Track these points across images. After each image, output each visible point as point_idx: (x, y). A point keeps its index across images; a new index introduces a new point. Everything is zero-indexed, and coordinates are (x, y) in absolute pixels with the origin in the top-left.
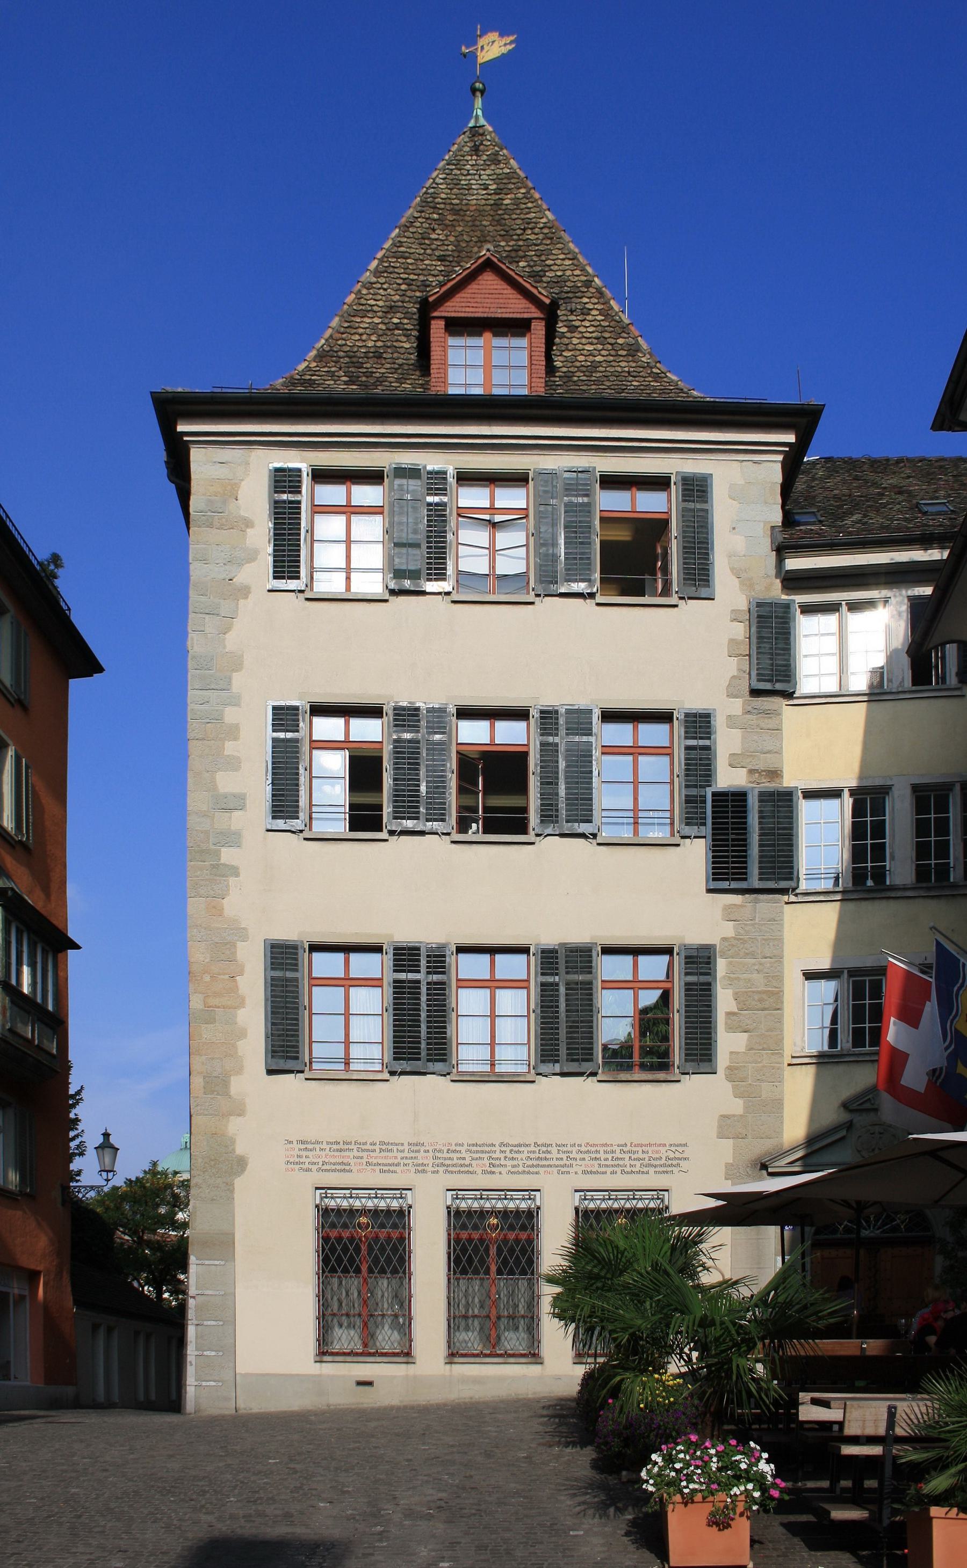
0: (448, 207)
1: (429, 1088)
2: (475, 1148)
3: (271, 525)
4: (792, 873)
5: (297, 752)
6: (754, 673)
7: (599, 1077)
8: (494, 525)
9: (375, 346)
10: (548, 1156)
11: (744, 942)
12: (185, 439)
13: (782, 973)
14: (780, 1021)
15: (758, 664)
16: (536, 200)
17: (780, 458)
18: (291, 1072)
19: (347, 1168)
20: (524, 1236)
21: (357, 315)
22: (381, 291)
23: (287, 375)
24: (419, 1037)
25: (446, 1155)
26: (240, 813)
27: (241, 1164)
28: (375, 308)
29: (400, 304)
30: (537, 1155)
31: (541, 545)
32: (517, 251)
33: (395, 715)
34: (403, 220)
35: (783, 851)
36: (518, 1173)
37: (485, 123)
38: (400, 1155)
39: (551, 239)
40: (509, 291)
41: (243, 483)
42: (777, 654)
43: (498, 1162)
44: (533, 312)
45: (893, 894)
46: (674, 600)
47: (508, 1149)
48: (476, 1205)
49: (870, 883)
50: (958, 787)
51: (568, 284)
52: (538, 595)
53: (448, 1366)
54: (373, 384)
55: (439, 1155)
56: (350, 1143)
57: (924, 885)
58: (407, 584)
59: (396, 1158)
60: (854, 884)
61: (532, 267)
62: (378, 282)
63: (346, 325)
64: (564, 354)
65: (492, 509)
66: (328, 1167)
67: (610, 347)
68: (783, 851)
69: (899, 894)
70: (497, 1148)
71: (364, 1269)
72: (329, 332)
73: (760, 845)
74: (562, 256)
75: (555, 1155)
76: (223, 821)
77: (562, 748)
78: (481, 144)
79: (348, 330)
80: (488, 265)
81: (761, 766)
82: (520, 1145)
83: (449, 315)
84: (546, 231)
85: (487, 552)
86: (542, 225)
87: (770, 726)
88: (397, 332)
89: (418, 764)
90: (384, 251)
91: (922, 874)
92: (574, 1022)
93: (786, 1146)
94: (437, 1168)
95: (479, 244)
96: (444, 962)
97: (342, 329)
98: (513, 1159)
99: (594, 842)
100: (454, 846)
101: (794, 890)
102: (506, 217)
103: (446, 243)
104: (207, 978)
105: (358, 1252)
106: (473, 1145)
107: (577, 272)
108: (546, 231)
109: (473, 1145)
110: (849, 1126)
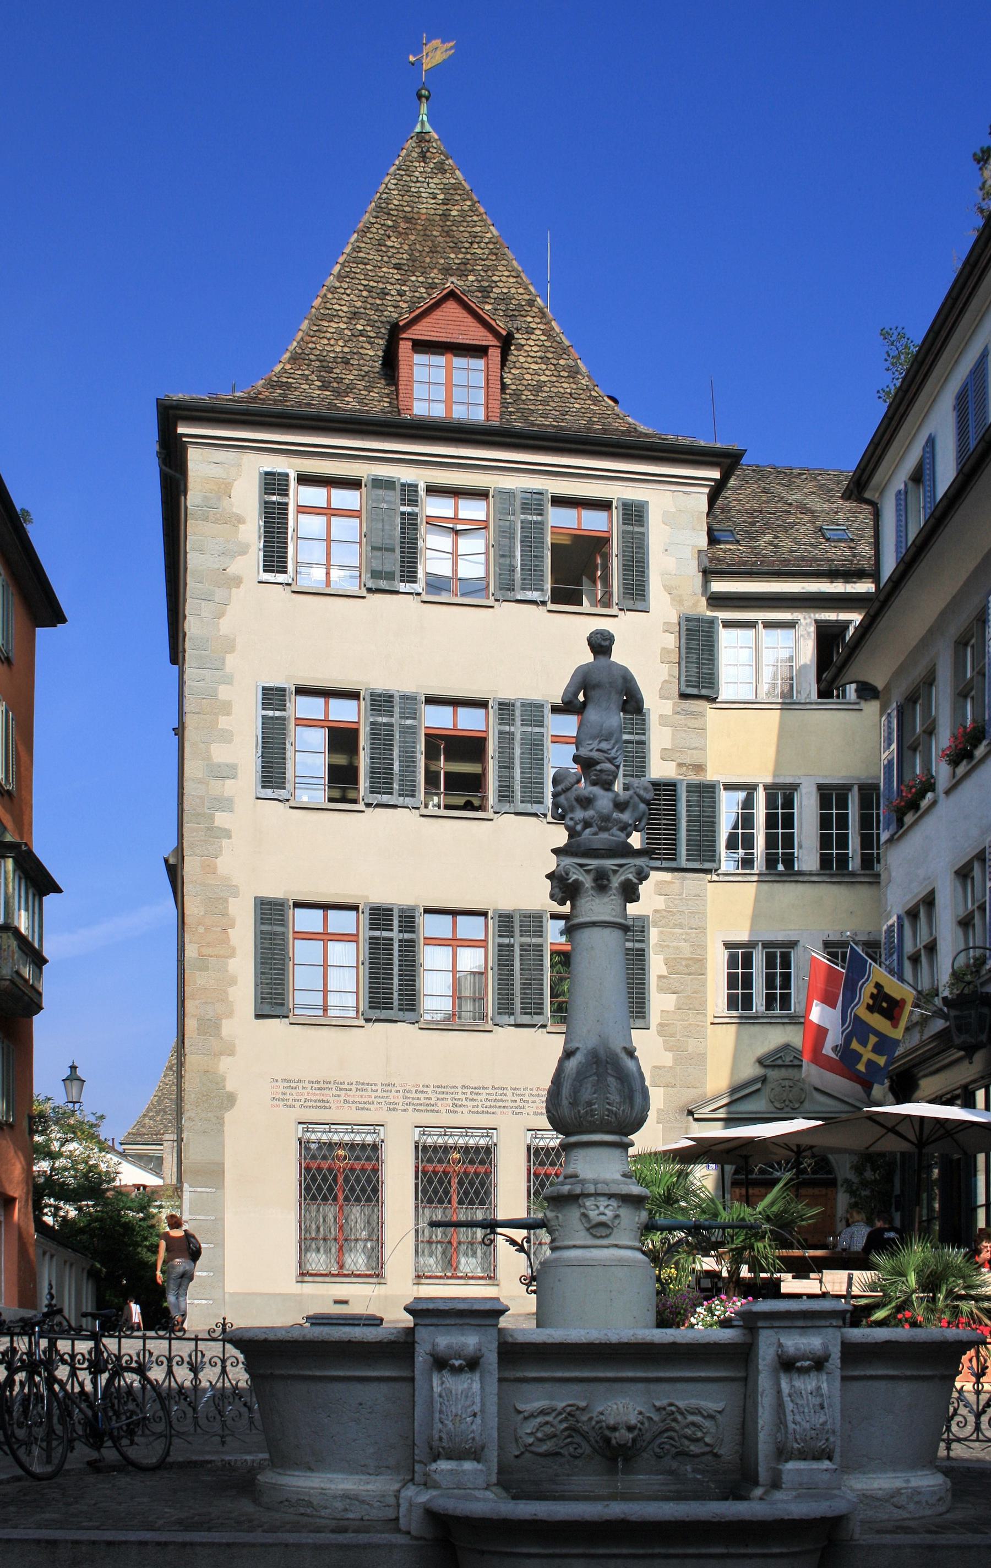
0: (401, 214)
1: (396, 1036)
2: (440, 1090)
3: (262, 523)
4: (714, 856)
5: (284, 729)
6: (683, 678)
7: (549, 1029)
8: (457, 533)
9: (342, 352)
10: (504, 1098)
11: (674, 914)
12: (184, 439)
13: (706, 942)
14: (704, 984)
15: (687, 671)
16: (481, 214)
17: (707, 490)
18: (278, 1017)
19: (327, 1105)
20: (482, 1169)
21: (328, 323)
22: (345, 296)
23: (266, 376)
24: (390, 989)
25: (414, 1095)
26: (233, 781)
27: (231, 1099)
28: (340, 313)
29: (362, 310)
30: (494, 1097)
31: (500, 552)
32: (465, 264)
33: (372, 700)
34: (361, 225)
35: (707, 836)
36: (478, 1112)
37: (431, 130)
38: (374, 1094)
39: (496, 254)
40: (469, 320)
41: (236, 483)
42: (703, 664)
43: (460, 1103)
44: (490, 340)
45: (801, 879)
46: (614, 611)
47: (469, 1091)
48: (440, 1141)
49: (781, 867)
50: (856, 789)
51: (513, 301)
52: (497, 600)
53: (416, 1287)
54: (345, 391)
55: (409, 1095)
56: (330, 1083)
57: (828, 872)
58: (383, 584)
59: (370, 1096)
60: (767, 868)
61: (480, 281)
62: (341, 287)
63: (315, 328)
64: (513, 371)
65: (456, 519)
66: (310, 1104)
67: (553, 368)
68: (707, 836)
69: (806, 879)
70: (459, 1090)
71: (341, 1197)
72: (300, 334)
73: (688, 831)
74: (506, 273)
75: (510, 1097)
76: (216, 787)
77: (518, 737)
78: (428, 151)
79: (317, 334)
80: (452, 295)
81: (688, 761)
82: (479, 1088)
84: (491, 246)
85: (450, 556)
86: (487, 240)
87: (696, 726)
88: (361, 339)
89: (392, 745)
90: (345, 256)
91: (825, 862)
92: (527, 979)
93: (709, 1094)
94: (406, 1107)
95: (431, 255)
96: (414, 922)
97: (312, 333)
98: (473, 1100)
99: (545, 820)
100: (422, 819)
101: (716, 870)
102: (455, 228)
103: (401, 251)
104: (201, 929)
105: (336, 1179)
106: (438, 1087)
107: (521, 291)
108: (491, 246)
109: (438, 1087)
110: (764, 1079)
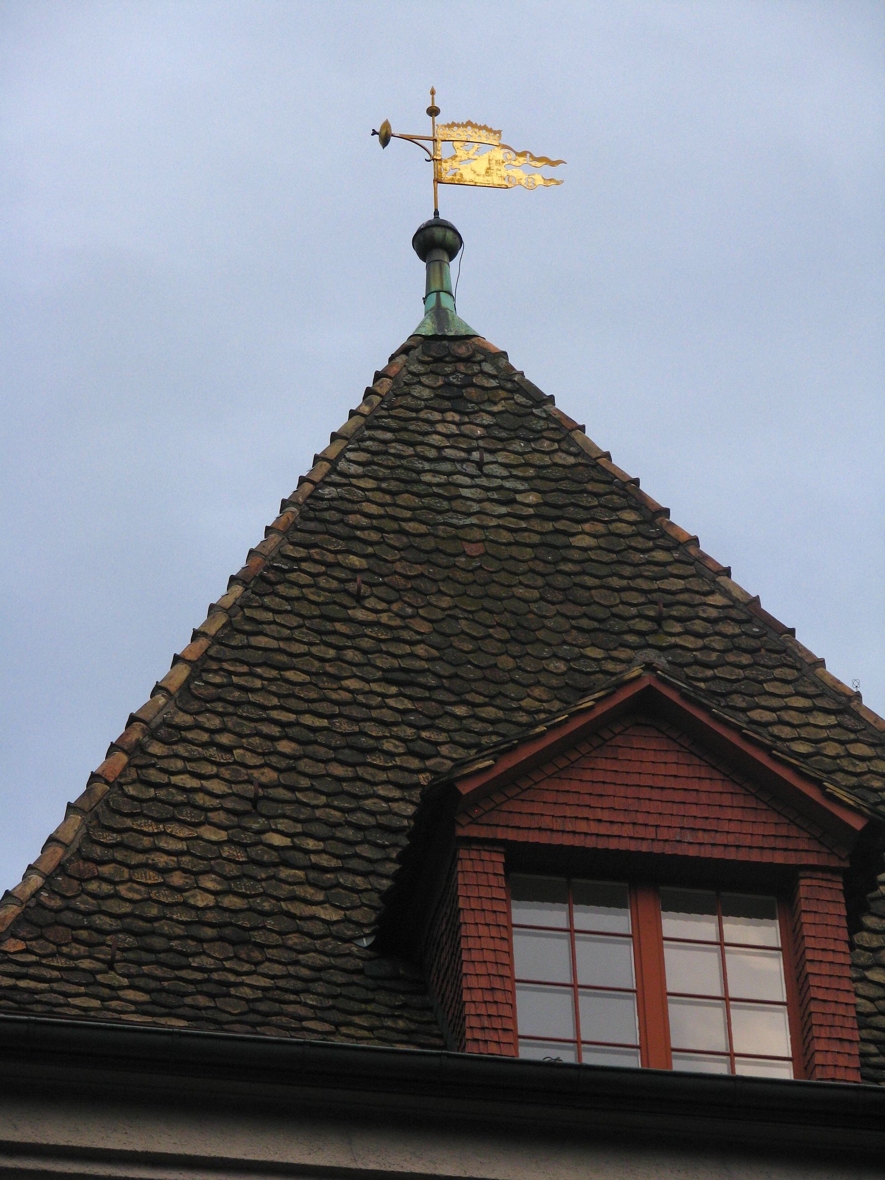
9: (218, 907)
22: (212, 751)
28: (200, 799)
83: (511, 835)
84: (730, 629)
97: (98, 851)
108: (730, 629)
